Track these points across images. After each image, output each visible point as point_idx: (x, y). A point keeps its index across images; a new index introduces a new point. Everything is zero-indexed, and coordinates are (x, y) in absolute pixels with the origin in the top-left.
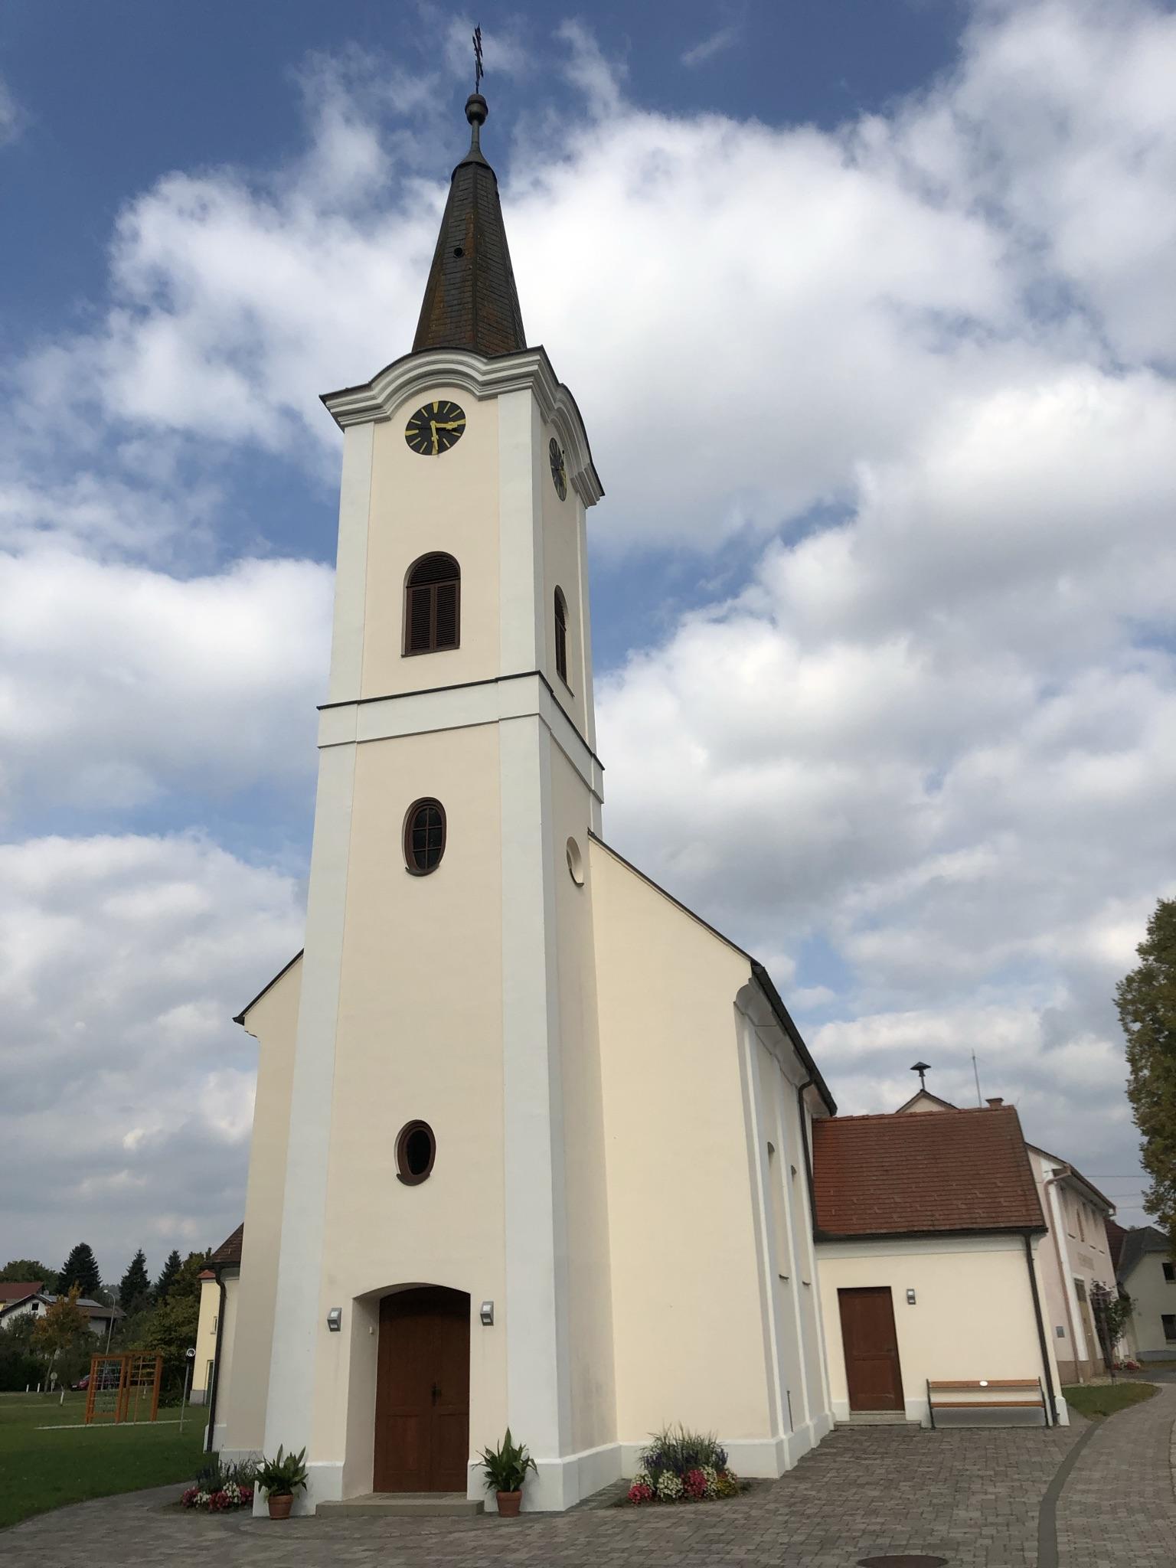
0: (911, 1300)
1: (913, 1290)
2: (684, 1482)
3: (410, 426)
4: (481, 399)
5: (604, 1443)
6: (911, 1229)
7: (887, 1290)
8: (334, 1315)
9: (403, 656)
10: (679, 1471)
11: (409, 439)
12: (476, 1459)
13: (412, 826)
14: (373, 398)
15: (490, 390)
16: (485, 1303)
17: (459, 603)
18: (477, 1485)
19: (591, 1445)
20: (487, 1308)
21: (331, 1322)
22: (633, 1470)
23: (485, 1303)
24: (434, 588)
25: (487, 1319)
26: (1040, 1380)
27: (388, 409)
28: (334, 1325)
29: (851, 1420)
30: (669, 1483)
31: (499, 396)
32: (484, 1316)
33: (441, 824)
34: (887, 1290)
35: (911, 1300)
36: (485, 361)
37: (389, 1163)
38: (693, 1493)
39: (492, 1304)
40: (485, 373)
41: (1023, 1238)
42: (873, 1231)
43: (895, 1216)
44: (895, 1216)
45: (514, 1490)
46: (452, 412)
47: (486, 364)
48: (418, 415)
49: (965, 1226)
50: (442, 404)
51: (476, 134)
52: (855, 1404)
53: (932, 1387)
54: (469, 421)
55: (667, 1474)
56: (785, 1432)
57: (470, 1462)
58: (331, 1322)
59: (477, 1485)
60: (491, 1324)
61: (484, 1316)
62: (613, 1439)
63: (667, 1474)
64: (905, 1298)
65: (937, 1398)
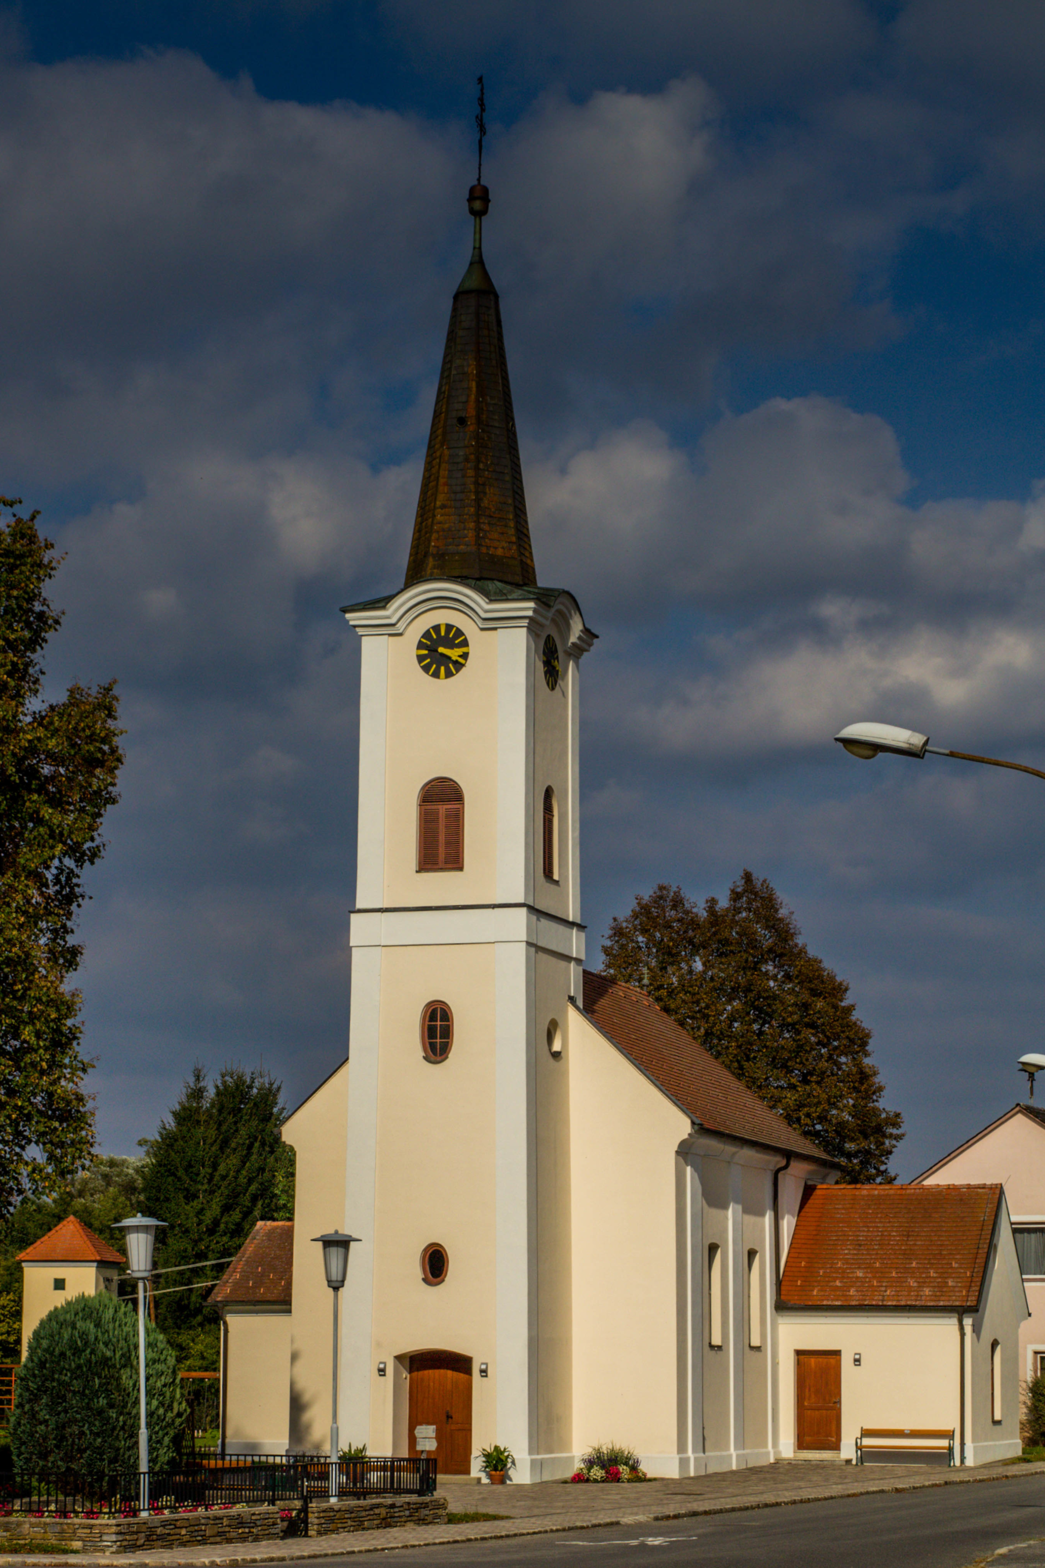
0: (857, 1362)
1: (860, 1354)
2: (607, 1472)
3: (420, 646)
4: (482, 629)
5: (562, 1452)
6: (862, 1303)
7: (837, 1353)
8: (382, 1366)
9: (417, 872)
10: (603, 1467)
11: (420, 659)
12: (476, 1452)
13: (427, 1019)
14: (388, 617)
15: (491, 624)
16: (482, 1364)
17: (463, 813)
18: (477, 1468)
19: (551, 1452)
20: (484, 1367)
21: (380, 1370)
22: (578, 1465)
23: (482, 1364)
24: (442, 809)
25: (484, 1372)
26: (954, 1431)
27: (401, 627)
28: (382, 1372)
29: (795, 1457)
30: (597, 1473)
31: (499, 630)
32: (482, 1371)
33: (448, 1021)
34: (837, 1353)
35: (857, 1362)
36: (487, 601)
37: (416, 1270)
38: (613, 1477)
39: (487, 1364)
40: (486, 611)
41: (956, 1315)
42: (830, 1303)
43: (932, 1271)
44: (932, 1271)
45: (502, 1470)
46: (453, 637)
47: (487, 603)
48: (427, 635)
49: (909, 1303)
50: (449, 627)
51: (477, 236)
52: (802, 1444)
53: (867, 1433)
54: (472, 649)
55: (595, 1468)
56: (694, 1451)
57: (473, 1456)
58: (380, 1370)
59: (477, 1468)
60: (486, 1376)
61: (482, 1371)
62: (571, 1451)
63: (595, 1468)
64: (852, 1361)
65: (867, 1442)
